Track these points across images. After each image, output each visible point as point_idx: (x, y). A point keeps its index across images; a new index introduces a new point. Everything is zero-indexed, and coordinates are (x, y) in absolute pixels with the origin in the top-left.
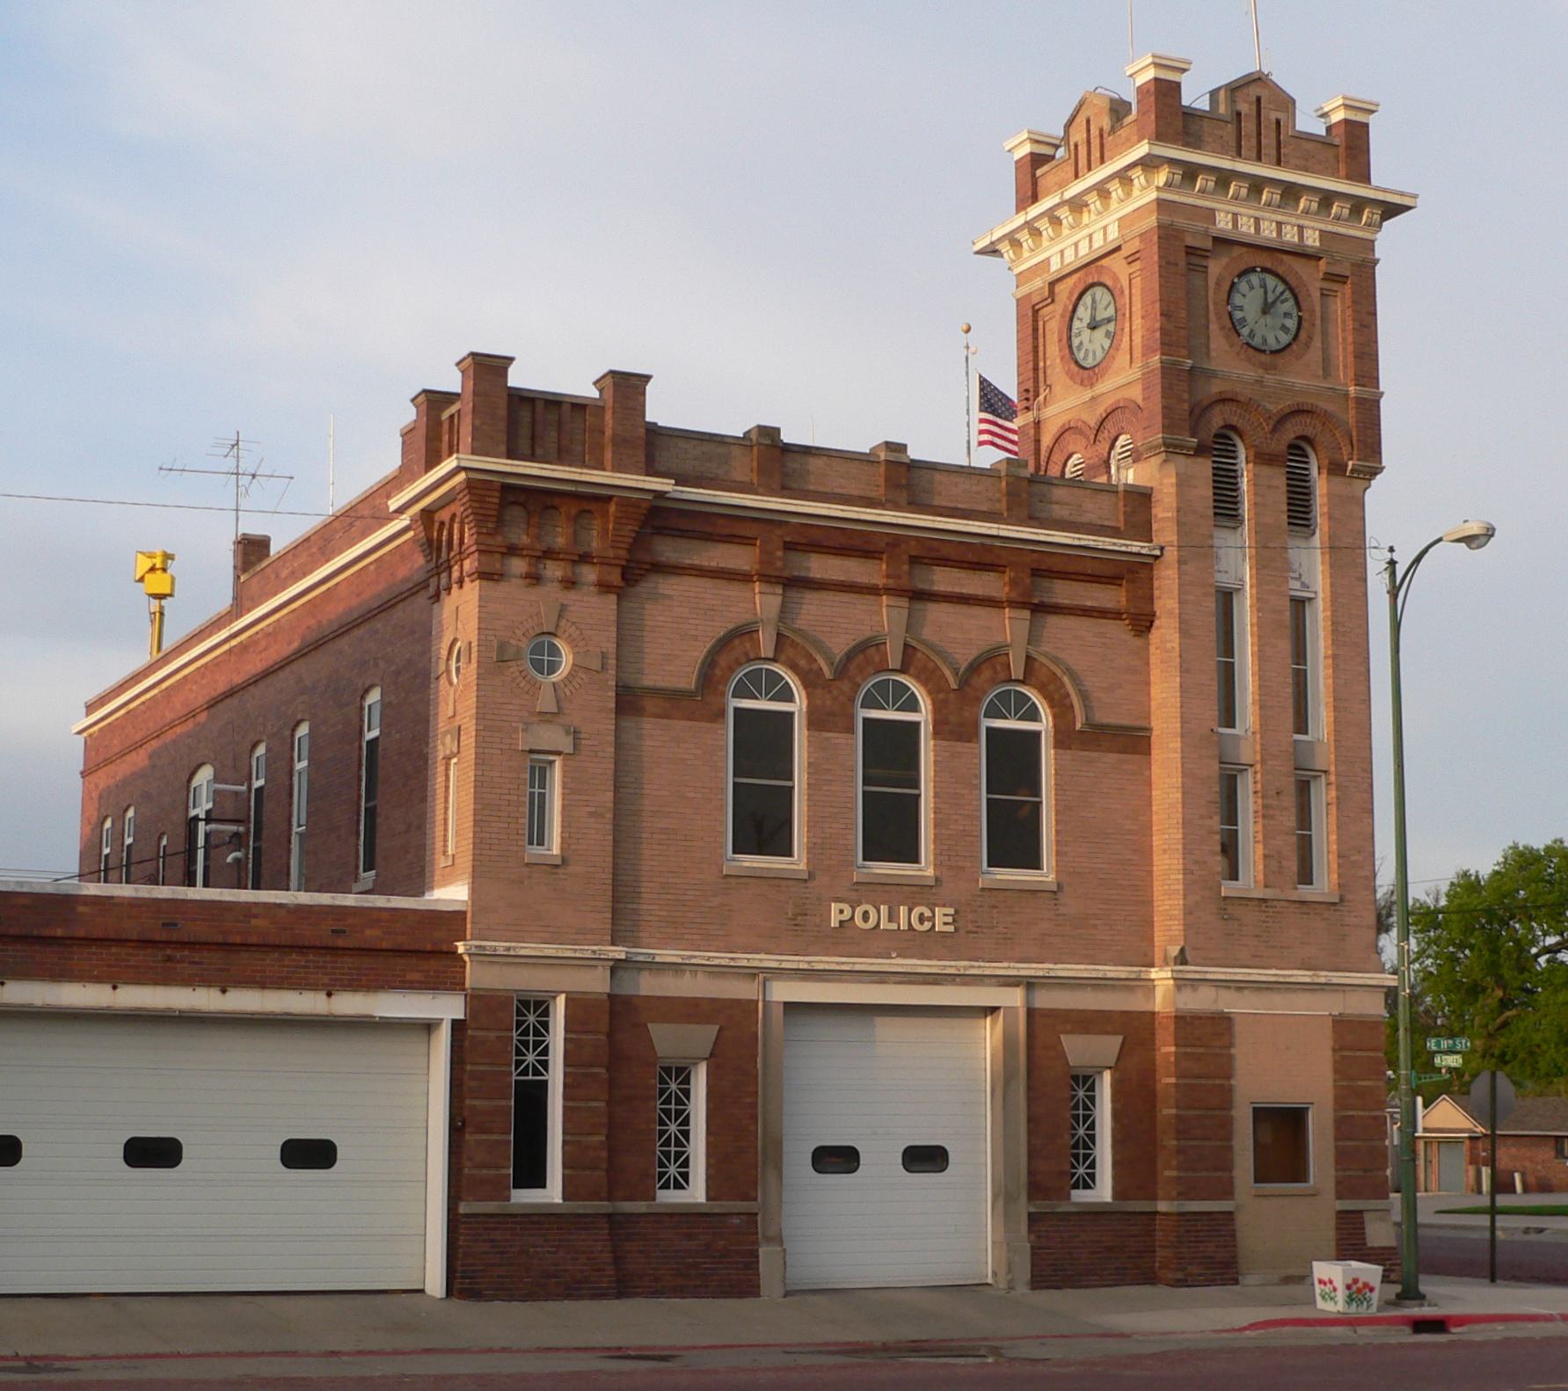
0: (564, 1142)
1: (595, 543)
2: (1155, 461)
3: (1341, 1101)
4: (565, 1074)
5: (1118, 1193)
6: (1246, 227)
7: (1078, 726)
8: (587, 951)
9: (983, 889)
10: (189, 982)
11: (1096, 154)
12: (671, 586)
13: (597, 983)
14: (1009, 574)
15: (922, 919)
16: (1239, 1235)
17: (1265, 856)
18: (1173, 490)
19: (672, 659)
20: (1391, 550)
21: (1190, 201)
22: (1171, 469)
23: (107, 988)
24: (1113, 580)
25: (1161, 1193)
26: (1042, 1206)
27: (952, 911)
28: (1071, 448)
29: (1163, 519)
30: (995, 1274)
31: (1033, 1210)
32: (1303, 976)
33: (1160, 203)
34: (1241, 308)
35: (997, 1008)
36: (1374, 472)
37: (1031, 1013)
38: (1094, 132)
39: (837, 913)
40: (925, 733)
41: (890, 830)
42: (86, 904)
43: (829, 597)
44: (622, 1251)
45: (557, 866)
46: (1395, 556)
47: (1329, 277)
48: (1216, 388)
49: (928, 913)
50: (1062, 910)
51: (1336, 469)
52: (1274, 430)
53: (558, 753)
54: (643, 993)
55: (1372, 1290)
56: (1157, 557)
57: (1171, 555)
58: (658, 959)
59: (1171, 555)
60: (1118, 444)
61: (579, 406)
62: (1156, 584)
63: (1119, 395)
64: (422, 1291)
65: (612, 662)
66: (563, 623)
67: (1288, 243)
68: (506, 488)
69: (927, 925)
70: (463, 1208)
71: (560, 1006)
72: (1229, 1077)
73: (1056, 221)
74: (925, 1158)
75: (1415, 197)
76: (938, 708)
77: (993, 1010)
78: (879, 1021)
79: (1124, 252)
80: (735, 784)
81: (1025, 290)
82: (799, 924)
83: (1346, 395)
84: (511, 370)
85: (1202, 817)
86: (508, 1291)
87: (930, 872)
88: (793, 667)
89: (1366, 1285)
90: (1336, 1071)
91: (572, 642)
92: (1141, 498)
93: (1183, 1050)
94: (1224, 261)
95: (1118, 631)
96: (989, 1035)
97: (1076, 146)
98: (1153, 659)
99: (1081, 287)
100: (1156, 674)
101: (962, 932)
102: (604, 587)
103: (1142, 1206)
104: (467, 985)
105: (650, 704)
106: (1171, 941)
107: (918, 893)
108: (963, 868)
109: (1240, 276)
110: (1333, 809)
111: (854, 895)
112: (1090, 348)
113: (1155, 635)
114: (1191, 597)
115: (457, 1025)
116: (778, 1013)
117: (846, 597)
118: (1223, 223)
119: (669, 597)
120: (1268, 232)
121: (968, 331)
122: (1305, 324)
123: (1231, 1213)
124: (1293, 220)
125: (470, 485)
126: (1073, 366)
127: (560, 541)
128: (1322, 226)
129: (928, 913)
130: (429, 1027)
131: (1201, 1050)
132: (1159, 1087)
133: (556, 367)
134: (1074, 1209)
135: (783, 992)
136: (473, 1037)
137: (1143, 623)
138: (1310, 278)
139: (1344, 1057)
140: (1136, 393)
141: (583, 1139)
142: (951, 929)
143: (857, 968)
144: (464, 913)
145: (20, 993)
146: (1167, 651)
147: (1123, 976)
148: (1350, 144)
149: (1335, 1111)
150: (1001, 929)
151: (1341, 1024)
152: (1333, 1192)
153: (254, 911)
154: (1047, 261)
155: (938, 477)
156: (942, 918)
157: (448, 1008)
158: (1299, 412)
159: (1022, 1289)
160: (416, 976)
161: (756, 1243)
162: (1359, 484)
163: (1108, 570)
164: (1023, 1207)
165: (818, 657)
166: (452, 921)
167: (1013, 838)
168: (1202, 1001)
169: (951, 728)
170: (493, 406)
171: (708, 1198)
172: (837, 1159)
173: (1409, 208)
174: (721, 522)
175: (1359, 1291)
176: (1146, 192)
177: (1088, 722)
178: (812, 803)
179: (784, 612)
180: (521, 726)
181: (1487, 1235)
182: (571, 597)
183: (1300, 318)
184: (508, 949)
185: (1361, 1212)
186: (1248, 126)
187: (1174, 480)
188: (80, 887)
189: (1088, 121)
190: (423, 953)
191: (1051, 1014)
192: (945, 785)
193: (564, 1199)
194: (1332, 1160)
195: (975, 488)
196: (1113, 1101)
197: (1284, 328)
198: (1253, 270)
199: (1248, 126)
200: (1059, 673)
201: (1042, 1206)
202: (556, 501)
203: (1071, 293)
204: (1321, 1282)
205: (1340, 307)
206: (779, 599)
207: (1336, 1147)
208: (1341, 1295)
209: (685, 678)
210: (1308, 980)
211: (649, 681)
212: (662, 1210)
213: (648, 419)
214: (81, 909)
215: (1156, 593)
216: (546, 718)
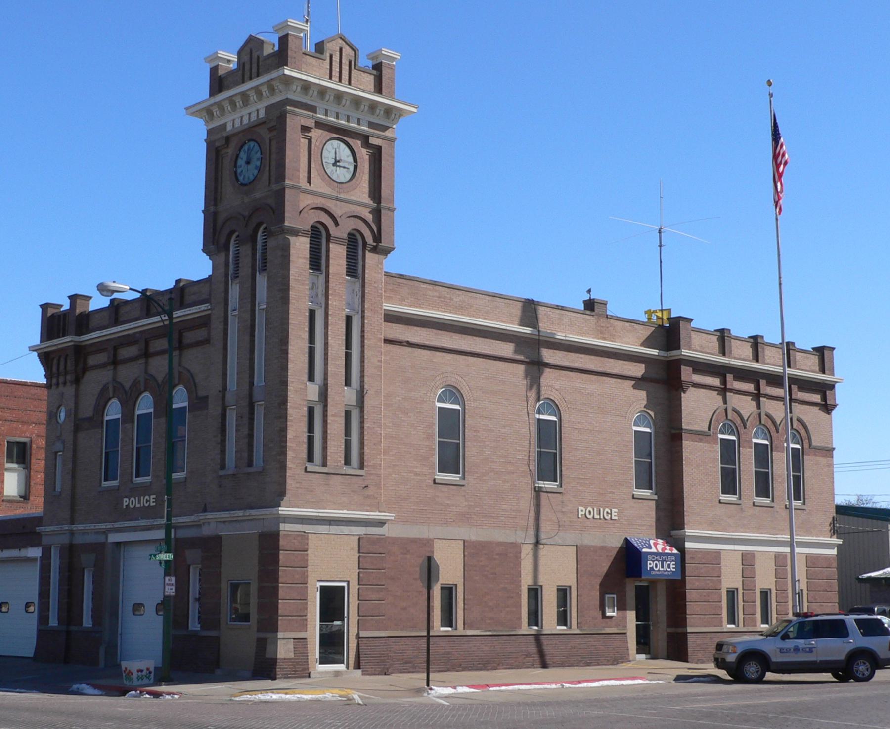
130: (33, 560)
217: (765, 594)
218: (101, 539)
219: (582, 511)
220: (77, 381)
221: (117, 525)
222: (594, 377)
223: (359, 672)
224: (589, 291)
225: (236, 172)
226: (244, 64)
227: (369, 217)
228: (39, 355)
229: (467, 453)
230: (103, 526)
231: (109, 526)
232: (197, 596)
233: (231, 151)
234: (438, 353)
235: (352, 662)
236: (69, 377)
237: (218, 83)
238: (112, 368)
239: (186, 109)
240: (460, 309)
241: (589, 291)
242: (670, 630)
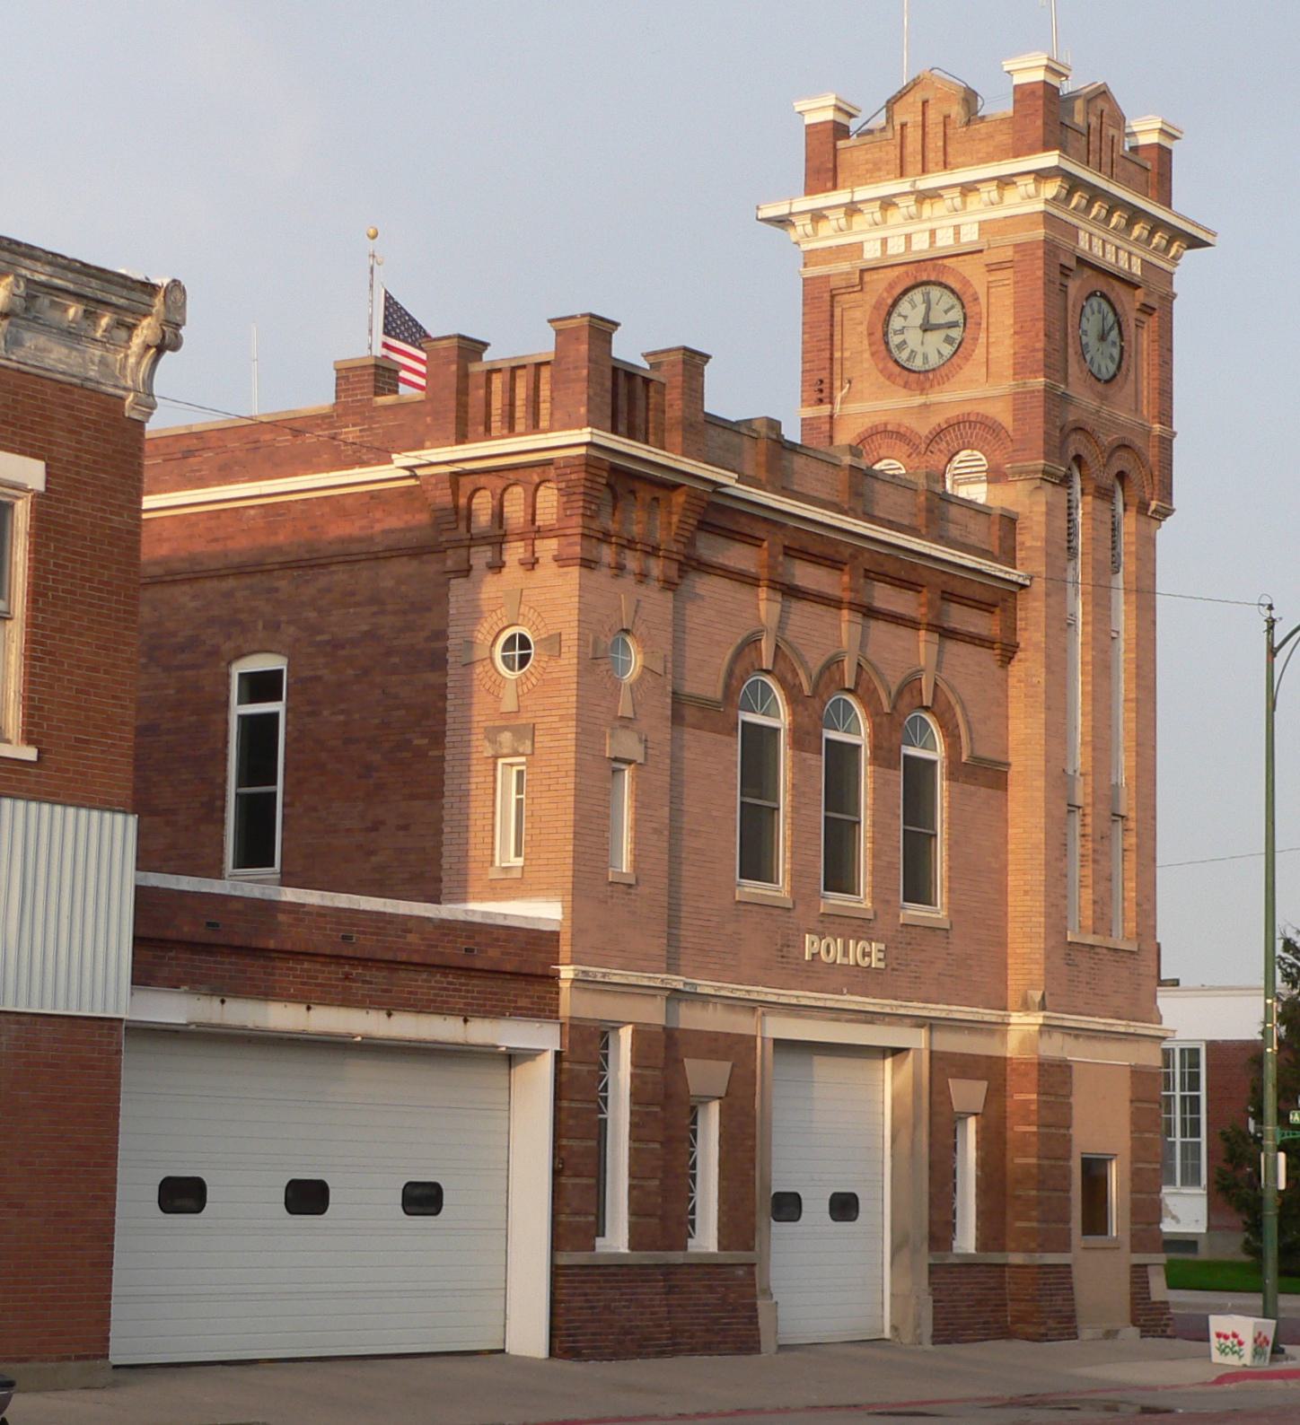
0: (631, 1188)
1: (659, 536)
2: (1028, 486)
4: (632, 1113)
5: (982, 1244)
7: (964, 759)
9: (903, 925)
10: (347, 1001)
11: (935, 142)
13: (653, 1013)
14: (926, 594)
16: (1076, 1290)
17: (1095, 902)
18: (1043, 519)
20: (1270, 607)
22: (1042, 498)
23: (216, 1002)
25: (1012, 1245)
28: (882, 452)
29: (1030, 548)
30: (894, 1328)
33: (1048, 218)
35: (907, 1050)
36: (1165, 512)
38: (934, 116)
40: (865, 754)
42: (284, 912)
45: (630, 886)
46: (1275, 615)
51: (1143, 508)
53: (629, 762)
54: (681, 1026)
56: (1023, 586)
57: (1039, 587)
58: (699, 990)
59: (1039, 587)
60: (957, 458)
62: (1020, 614)
63: (967, 408)
64: (503, 1351)
68: (614, 469)
71: (626, 1034)
72: (1069, 1127)
74: (844, 1207)
75: (1214, 235)
76: (876, 731)
77: (896, 1052)
79: (987, 258)
81: (813, 271)
83: (1150, 431)
84: (616, 337)
87: (943, 914)
88: (782, 682)
91: (642, 643)
92: (1009, 522)
93: (1044, 1098)
95: (988, 658)
96: (889, 1081)
97: (903, 126)
98: (1012, 692)
99: (908, 282)
100: (1016, 708)
101: (889, 968)
103: (996, 1258)
104: (561, 1013)
106: (1032, 986)
107: (857, 927)
109: (1087, 299)
110: (1132, 856)
112: (920, 350)
113: (1016, 668)
116: (770, 1046)
119: (702, 598)
121: (374, 237)
123: (1068, 1266)
125: (590, 464)
126: (891, 365)
127: (636, 530)
130: (512, 1058)
131: (1052, 1099)
132: (1009, 1135)
134: (957, 1261)
136: (571, 1070)
137: (1008, 652)
138: (1130, 303)
139: (1137, 1108)
140: (1002, 414)
141: (645, 1183)
142: (882, 965)
143: (804, 1002)
144: (556, 934)
146: (1033, 686)
147: (993, 1019)
148: (1155, 170)
149: (1132, 1163)
150: (913, 967)
153: (410, 925)
154: (859, 247)
155: (878, 486)
157: (544, 1038)
158: (1124, 447)
159: (928, 1346)
161: (755, 1296)
162: (1154, 523)
163: (986, 596)
165: (801, 672)
166: (542, 942)
168: (1054, 1048)
169: (884, 755)
171: (721, 1246)
172: (183, 1195)
173: (1207, 244)
174: (743, 520)
176: (1028, 201)
177: (972, 757)
178: (795, 827)
179: (782, 624)
180: (608, 731)
183: (1122, 348)
184: (604, 975)
185: (1146, 1266)
186: (913, 136)
187: (1043, 509)
188: (280, 894)
189: (925, 103)
190: (511, 972)
193: (631, 1247)
196: (978, 1148)
197: (949, 340)
199: (913, 136)
200: (953, 701)
202: (637, 485)
203: (891, 287)
204: (1219, 1335)
205: (1145, 340)
207: (1132, 1200)
208: (1248, 1349)
209: (716, 692)
212: (601, 1262)
214: (281, 917)
215: (1020, 624)
216: (626, 723)
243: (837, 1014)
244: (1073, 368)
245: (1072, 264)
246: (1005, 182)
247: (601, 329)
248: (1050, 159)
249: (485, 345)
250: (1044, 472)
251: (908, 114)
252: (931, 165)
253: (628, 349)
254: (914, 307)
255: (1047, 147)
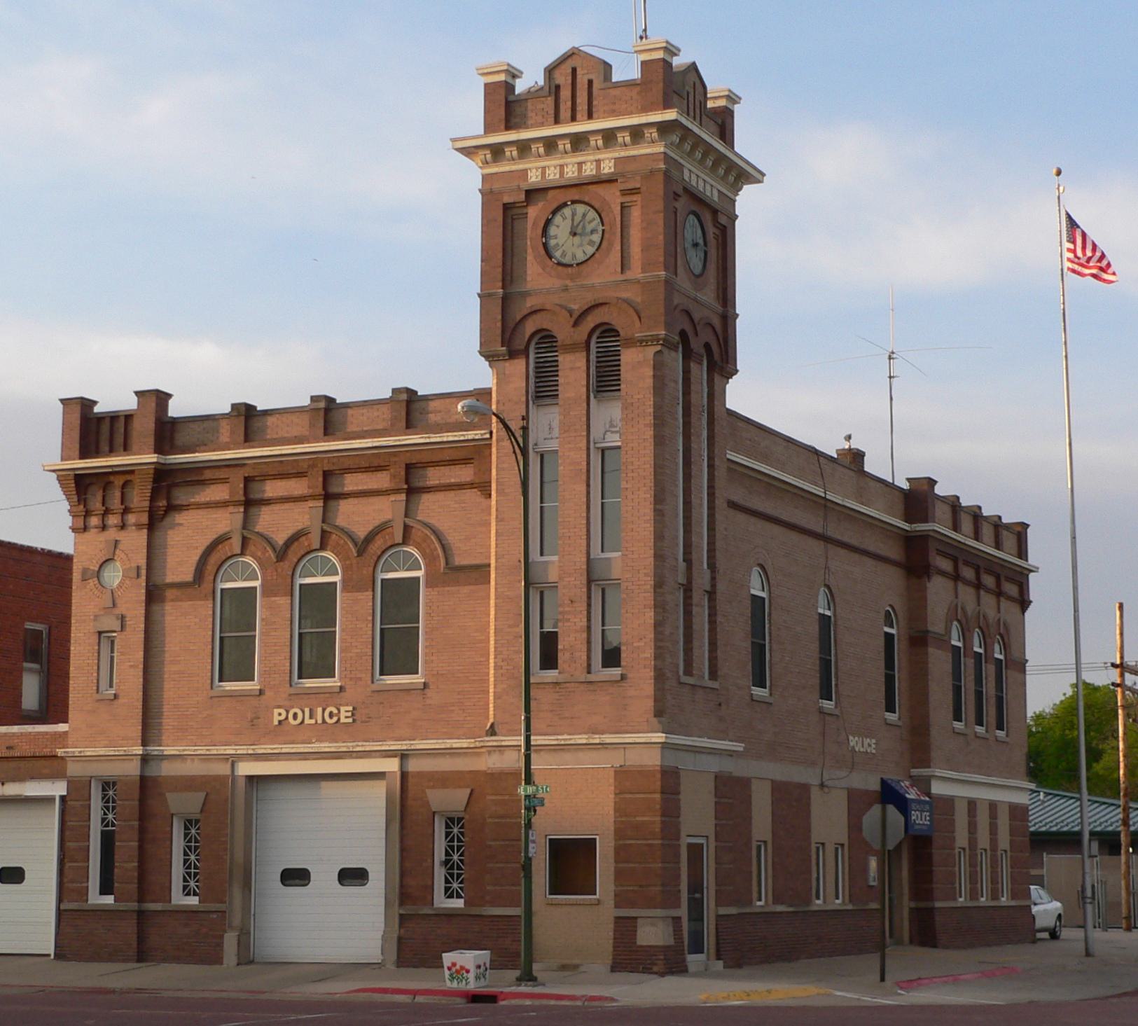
3: (620, 833)
6: (553, 175)
8: (121, 751)
12: (180, 518)
15: (331, 715)
19: (180, 561)
21: (507, 168)
24: (465, 461)
26: (409, 909)
27: (351, 708)
31: (402, 912)
32: (582, 739)
34: (556, 237)
37: (404, 775)
39: (277, 715)
41: (314, 656)
43: (351, 501)
44: (145, 936)
47: (625, 192)
48: (530, 303)
49: (335, 711)
50: (428, 702)
52: (575, 324)
55: (468, 971)
61: (128, 417)
65: (144, 572)
66: (118, 552)
67: (570, 179)
69: (335, 719)
70: (62, 907)
73: (716, 164)
78: (324, 784)
80: (382, 630)
82: (256, 726)
85: (510, 626)
86: (81, 957)
89: (462, 968)
90: (616, 810)
94: (541, 205)
95: (472, 496)
96: (378, 792)
99: (547, 214)
102: (139, 526)
105: (170, 594)
108: (360, 679)
111: (287, 703)
114: (505, 466)
115: (63, 799)
117: (287, 506)
118: (534, 178)
120: (571, 173)
122: (606, 235)
124: (591, 158)
128: (616, 155)
129: (335, 711)
130: (49, 800)
133: (114, 397)
135: (245, 769)
142: (350, 720)
145: (11, 789)
151: (622, 774)
152: (612, 902)
155: (350, 412)
156: (345, 714)
157: (58, 789)
159: (391, 966)
160: (46, 771)
164: (396, 911)
167: (397, 651)
170: (312, 398)
172: (295, 877)
175: (457, 972)
181: (1083, 944)
182: (121, 536)
186: (565, 94)
191: (420, 775)
192: (355, 625)
194: (612, 877)
195: (376, 414)
197: (591, 243)
198: (565, 205)
199: (565, 94)
201: (409, 909)
206: (241, 515)
210: (584, 741)
211: (170, 579)
213: (170, 414)
217: (696, 852)
218: (223, 769)
219: (853, 741)
220: (154, 523)
221: (261, 749)
222: (856, 556)
223: (721, 963)
224: (849, 438)
225: (545, 245)
226: (558, 87)
227: (716, 322)
228: (59, 479)
229: (840, 664)
230: (230, 750)
231: (242, 750)
232: (443, 858)
233: (535, 213)
234: (753, 520)
235: (713, 951)
236: (131, 519)
237: (506, 104)
238: (242, 509)
239: (453, 140)
240: (765, 458)
241: (849, 438)
242: (913, 905)
243: (304, 756)
244: (680, 270)
245: (680, 191)
246: (637, 133)
247: (162, 398)
248: (671, 115)
249: (95, 403)
250: (664, 340)
251: (563, 78)
252: (579, 116)
253: (175, 409)
254: (564, 218)
255: (667, 105)
